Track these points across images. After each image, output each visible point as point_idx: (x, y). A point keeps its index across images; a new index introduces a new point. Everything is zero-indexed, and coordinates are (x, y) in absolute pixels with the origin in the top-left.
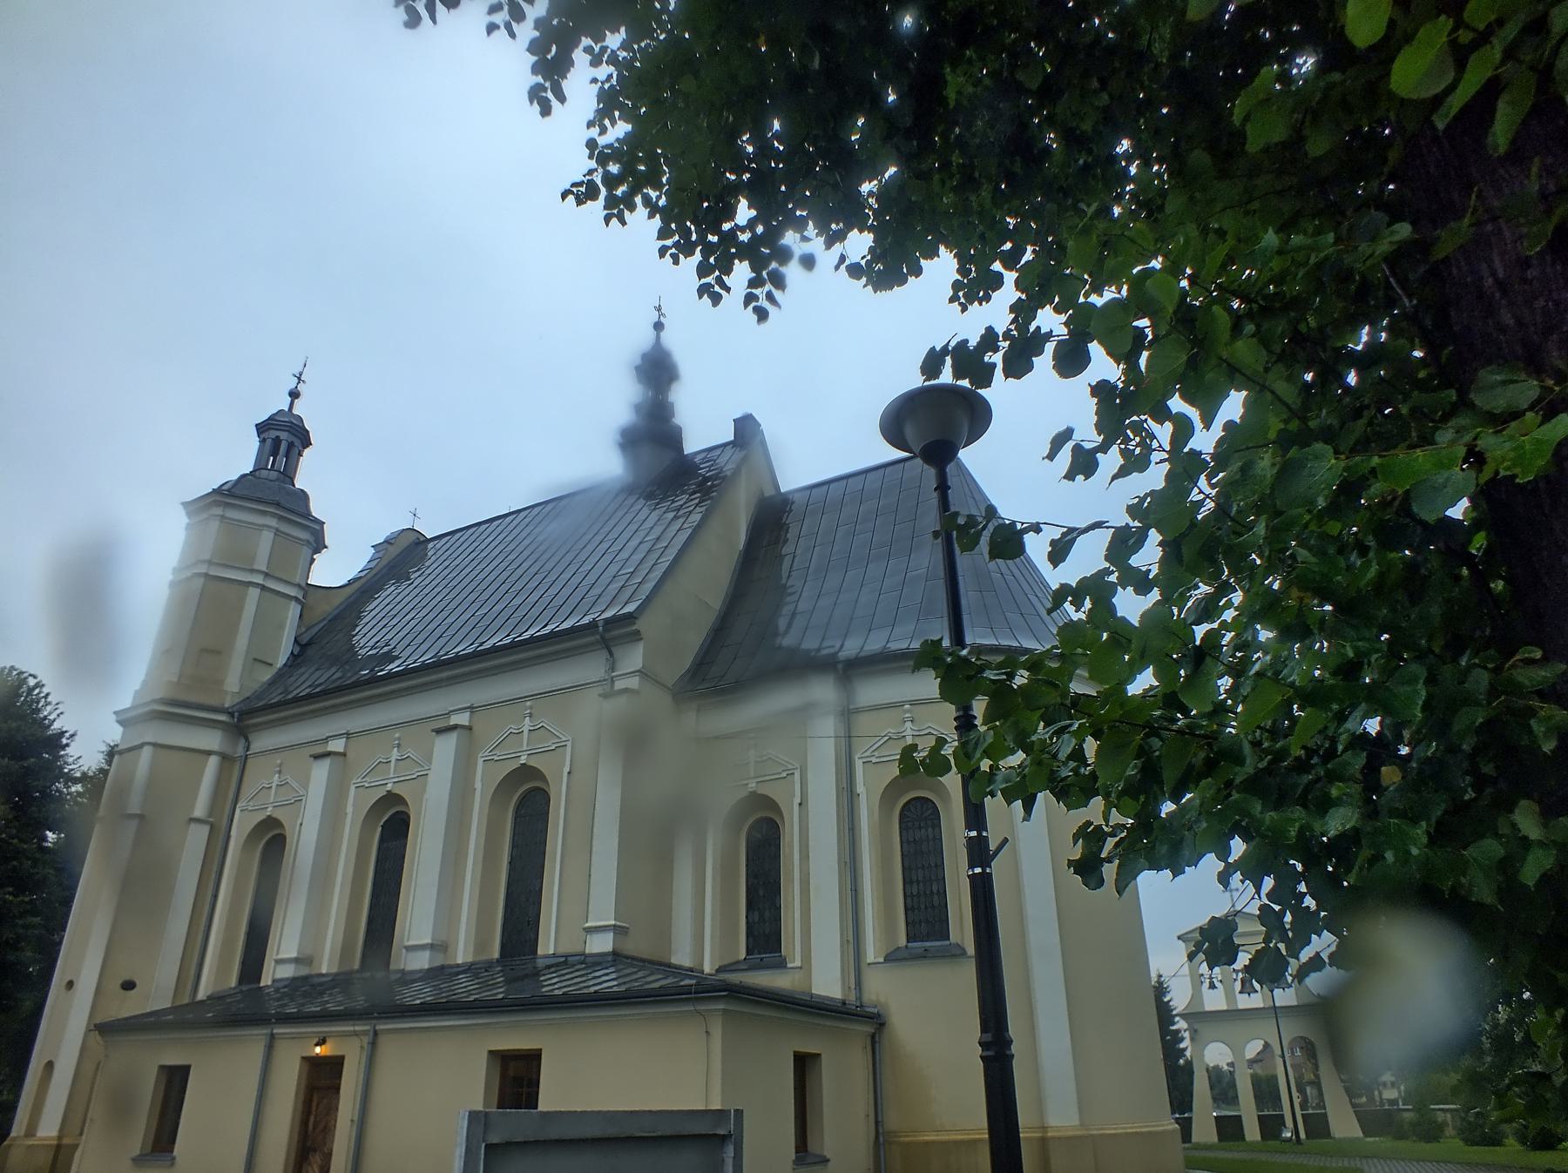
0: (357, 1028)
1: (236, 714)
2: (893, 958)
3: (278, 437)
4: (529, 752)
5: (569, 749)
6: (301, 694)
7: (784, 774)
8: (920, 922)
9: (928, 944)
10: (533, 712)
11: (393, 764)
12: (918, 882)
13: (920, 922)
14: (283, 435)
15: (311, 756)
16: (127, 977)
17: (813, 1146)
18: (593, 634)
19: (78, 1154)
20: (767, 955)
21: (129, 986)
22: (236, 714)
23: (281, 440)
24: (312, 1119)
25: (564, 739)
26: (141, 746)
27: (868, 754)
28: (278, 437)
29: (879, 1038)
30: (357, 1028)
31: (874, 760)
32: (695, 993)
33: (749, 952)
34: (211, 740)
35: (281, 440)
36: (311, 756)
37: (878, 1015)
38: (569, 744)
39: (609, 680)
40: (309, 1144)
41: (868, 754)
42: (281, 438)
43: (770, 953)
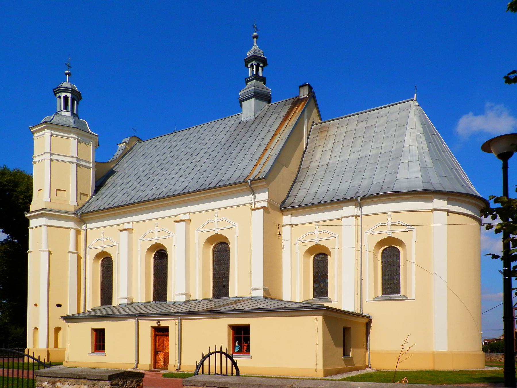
0: (174, 318)
1: (79, 214)
2: (376, 299)
3: (66, 96)
4: (104, 247)
5: (117, 246)
6: (157, 197)
7: (331, 238)
8: (388, 288)
9: (391, 295)
10: (158, 225)
11: (156, 232)
12: (388, 275)
13: (388, 288)
14: (69, 95)
15: (119, 230)
16: (35, 307)
17: (346, 354)
18: (245, 185)
19: (66, 353)
20: (322, 298)
21: (59, 305)
22: (79, 214)
23: (68, 97)
24: (157, 344)
25: (234, 224)
26: (41, 226)
27: (370, 231)
28: (66, 96)
29: (370, 323)
30: (174, 318)
31: (373, 233)
32: (313, 309)
33: (314, 296)
34: (71, 224)
35: (68, 97)
36: (119, 230)
37: (369, 317)
38: (117, 245)
39: (85, 230)
40: (157, 350)
41: (370, 231)
42: (68, 96)
43: (323, 297)
